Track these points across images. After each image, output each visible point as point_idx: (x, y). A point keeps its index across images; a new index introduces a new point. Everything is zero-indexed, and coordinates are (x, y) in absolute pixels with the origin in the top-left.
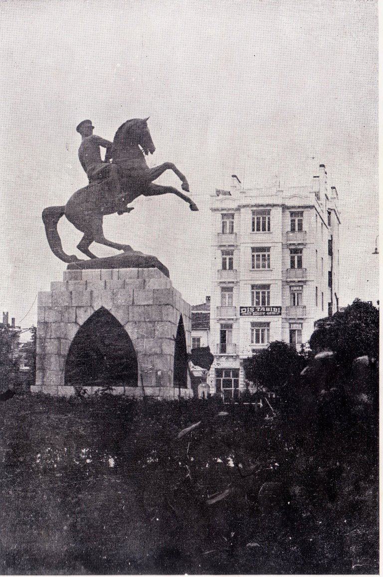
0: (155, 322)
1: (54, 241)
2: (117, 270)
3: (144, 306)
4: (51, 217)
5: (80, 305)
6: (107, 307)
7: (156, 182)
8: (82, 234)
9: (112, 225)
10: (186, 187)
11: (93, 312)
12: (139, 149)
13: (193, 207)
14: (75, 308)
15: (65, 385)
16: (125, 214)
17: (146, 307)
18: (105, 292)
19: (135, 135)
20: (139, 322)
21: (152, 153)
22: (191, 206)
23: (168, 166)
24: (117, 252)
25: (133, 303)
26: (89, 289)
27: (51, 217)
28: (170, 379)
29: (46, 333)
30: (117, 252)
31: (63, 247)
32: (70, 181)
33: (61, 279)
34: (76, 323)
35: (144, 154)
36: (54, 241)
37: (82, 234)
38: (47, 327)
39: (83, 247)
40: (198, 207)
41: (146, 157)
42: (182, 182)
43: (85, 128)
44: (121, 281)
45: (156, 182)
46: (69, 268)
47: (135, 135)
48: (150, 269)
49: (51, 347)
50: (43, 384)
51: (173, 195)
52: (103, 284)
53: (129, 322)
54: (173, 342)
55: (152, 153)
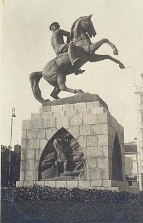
0: (97, 135)
1: (38, 94)
2: (73, 104)
3: (90, 125)
4: (36, 77)
5: (49, 127)
6: (65, 128)
7: (97, 52)
8: (54, 87)
9: (72, 81)
10: (116, 53)
11: (57, 131)
12: (86, 34)
13: (122, 66)
14: (45, 129)
15: (38, 180)
16: (79, 75)
17: (91, 126)
18: (62, 117)
19: (85, 28)
20: (87, 136)
21: (94, 36)
22: (120, 66)
23: (105, 41)
24: (73, 95)
25: (83, 123)
26: (54, 117)
27: (36, 77)
28: (103, 172)
29: (27, 146)
30: (73, 95)
31: (42, 95)
32: (46, 55)
33: (38, 112)
34: (46, 138)
35: (90, 37)
36: (38, 94)
37: (54, 87)
38: (28, 143)
39: (55, 94)
40: (119, 52)
41: (91, 39)
42: (118, 65)
43: (55, 26)
44: (75, 111)
45: (97, 52)
46: (43, 106)
47: (85, 28)
48: (95, 102)
49: (30, 155)
50: (24, 180)
51: (109, 60)
52: (63, 114)
53: (80, 136)
54: (108, 146)
55: (94, 36)
